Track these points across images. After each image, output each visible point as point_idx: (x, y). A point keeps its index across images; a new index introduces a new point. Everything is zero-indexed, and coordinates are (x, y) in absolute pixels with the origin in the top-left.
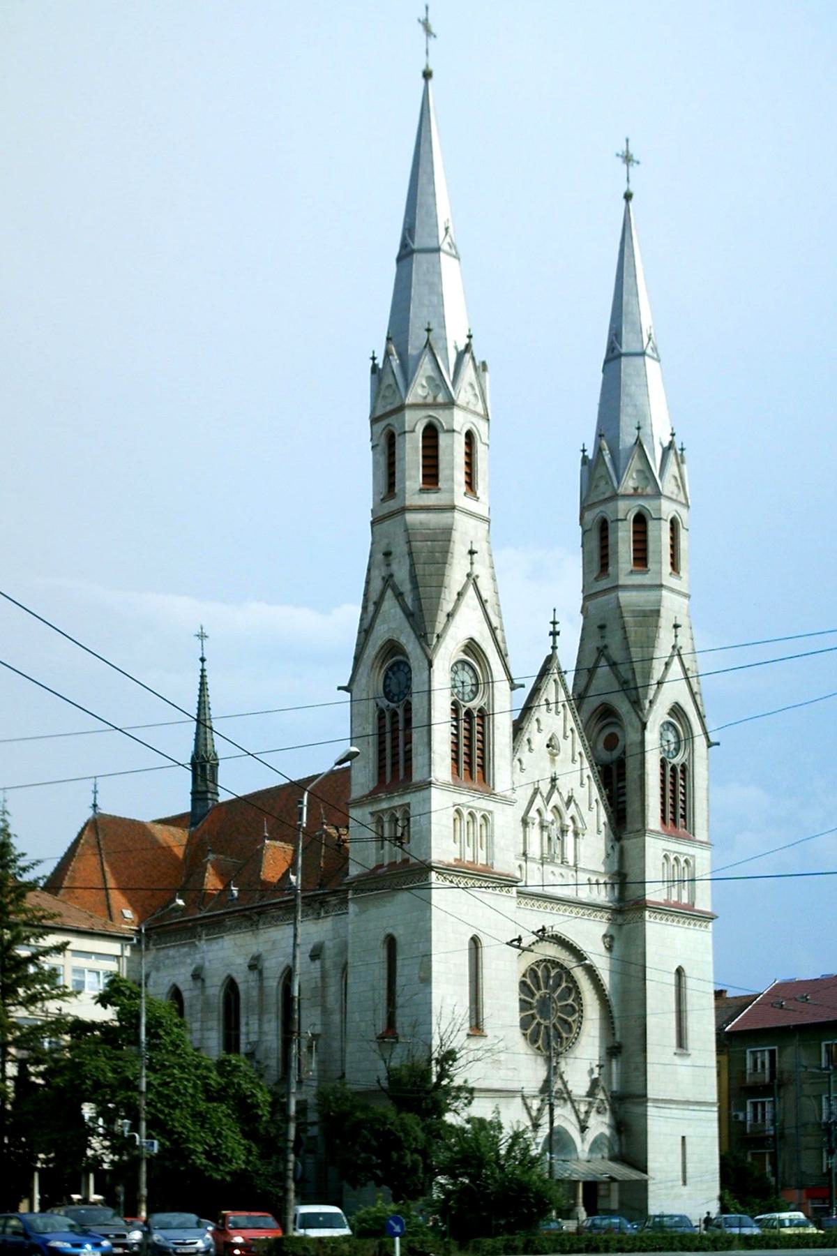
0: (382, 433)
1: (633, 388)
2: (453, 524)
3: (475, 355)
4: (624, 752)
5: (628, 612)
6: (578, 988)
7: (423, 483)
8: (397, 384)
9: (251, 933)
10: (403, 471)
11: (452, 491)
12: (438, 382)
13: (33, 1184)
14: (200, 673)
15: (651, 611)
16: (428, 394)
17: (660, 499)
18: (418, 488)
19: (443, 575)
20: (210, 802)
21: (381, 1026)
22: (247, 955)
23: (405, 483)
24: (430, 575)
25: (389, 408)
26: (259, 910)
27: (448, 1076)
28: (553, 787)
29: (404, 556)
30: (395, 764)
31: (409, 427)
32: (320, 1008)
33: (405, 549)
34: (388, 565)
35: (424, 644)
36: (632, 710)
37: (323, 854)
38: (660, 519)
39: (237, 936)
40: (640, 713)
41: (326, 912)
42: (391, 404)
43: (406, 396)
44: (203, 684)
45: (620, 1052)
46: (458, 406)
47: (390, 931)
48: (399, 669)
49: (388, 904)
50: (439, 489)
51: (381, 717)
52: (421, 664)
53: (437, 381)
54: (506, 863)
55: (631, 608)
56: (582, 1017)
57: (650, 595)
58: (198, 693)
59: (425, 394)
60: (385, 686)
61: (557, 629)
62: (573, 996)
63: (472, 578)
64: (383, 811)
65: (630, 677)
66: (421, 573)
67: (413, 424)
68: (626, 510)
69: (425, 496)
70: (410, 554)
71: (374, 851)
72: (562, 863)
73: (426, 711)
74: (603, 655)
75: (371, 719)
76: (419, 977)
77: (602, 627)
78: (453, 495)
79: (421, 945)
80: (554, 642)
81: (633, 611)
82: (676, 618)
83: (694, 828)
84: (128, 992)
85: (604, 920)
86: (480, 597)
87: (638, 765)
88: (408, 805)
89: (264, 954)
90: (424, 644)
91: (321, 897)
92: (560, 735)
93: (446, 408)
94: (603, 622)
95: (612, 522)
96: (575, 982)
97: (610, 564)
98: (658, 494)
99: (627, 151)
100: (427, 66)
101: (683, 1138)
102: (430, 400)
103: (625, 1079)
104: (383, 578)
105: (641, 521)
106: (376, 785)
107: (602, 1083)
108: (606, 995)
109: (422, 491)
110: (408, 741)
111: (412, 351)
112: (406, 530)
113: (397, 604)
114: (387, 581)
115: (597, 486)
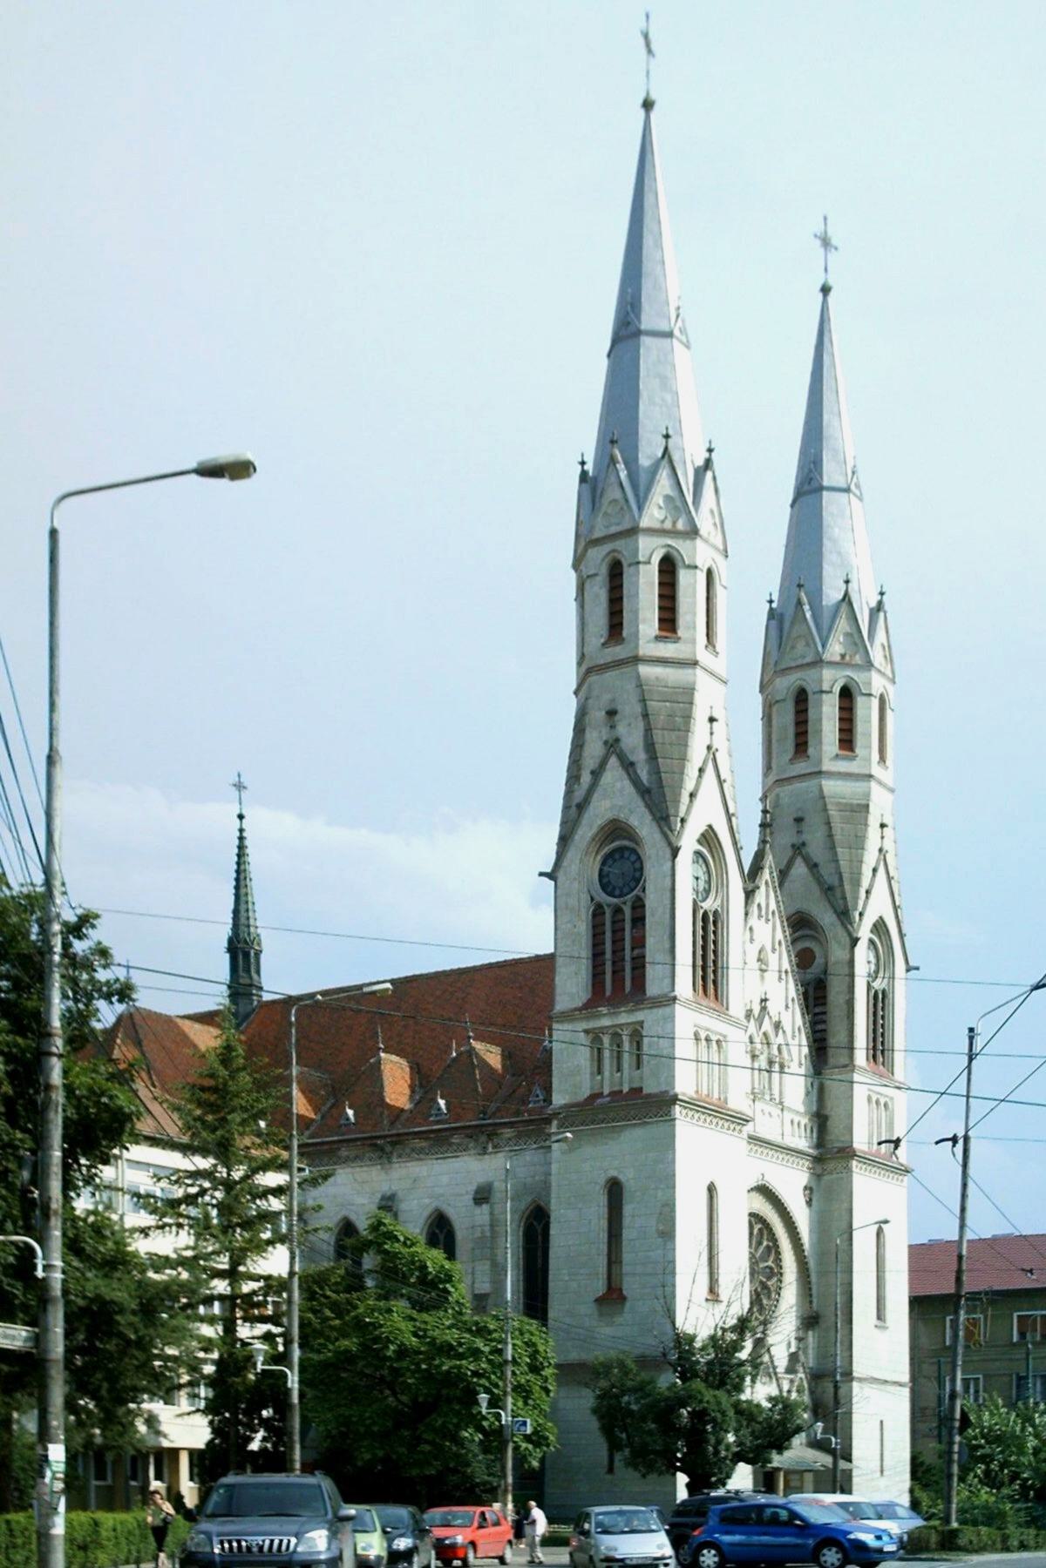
0: (603, 560)
1: (837, 530)
2: (694, 683)
3: (716, 474)
4: (825, 972)
5: (832, 804)
6: (778, 1247)
7: (660, 629)
8: (627, 501)
9: (379, 1167)
10: (636, 612)
11: (693, 642)
12: (679, 504)
14: (238, 834)
15: (858, 805)
16: (666, 518)
17: (870, 670)
18: (654, 635)
19: (686, 745)
20: (255, 998)
21: (600, 1287)
22: (373, 1194)
23: (638, 626)
24: (671, 744)
25: (613, 530)
26: (394, 1139)
27: (388, 1341)
28: (764, 1009)
29: (637, 717)
30: (618, 972)
31: (643, 556)
32: (488, 1263)
33: (638, 709)
34: (613, 727)
35: (666, 829)
36: (838, 923)
37: (478, 1077)
38: (870, 695)
39: (358, 1169)
40: (849, 926)
41: (495, 1147)
42: (618, 524)
43: (640, 516)
44: (241, 847)
45: (817, 1323)
46: (701, 537)
47: (613, 1173)
48: (622, 857)
49: (611, 1142)
50: (679, 638)
51: (598, 912)
52: (661, 853)
53: (677, 504)
54: (738, 1101)
55: (836, 800)
56: (781, 1282)
57: (858, 787)
58: (236, 859)
59: (662, 518)
60: (601, 876)
62: (772, 1259)
64: (603, 1030)
65: (836, 883)
66: (660, 741)
67: (648, 553)
68: (832, 680)
69: (661, 645)
70: (646, 716)
71: (588, 1076)
72: (771, 1100)
73: (668, 911)
74: (800, 853)
75: (584, 917)
76: (657, 1230)
77: (799, 820)
78: (695, 647)
79: (660, 1193)
81: (839, 804)
82: (882, 815)
83: (893, 1066)
84: (402, 1239)
85: (805, 1169)
86: (718, 776)
87: (844, 987)
88: (641, 1023)
89: (400, 1194)
90: (666, 829)
91: (490, 1128)
92: (769, 948)
93: (687, 538)
94: (800, 814)
95: (814, 693)
96: (776, 1240)
97: (810, 743)
98: (869, 665)
99: (826, 232)
100: (648, 94)
101: (882, 1422)
102: (668, 525)
103: (824, 1353)
104: (606, 743)
105: (847, 694)
106: (589, 996)
107: (802, 1358)
108: (805, 1257)
109: (657, 638)
110: (639, 942)
111: (645, 461)
112: (640, 686)
113: (626, 776)
114: (612, 746)
115: (793, 647)
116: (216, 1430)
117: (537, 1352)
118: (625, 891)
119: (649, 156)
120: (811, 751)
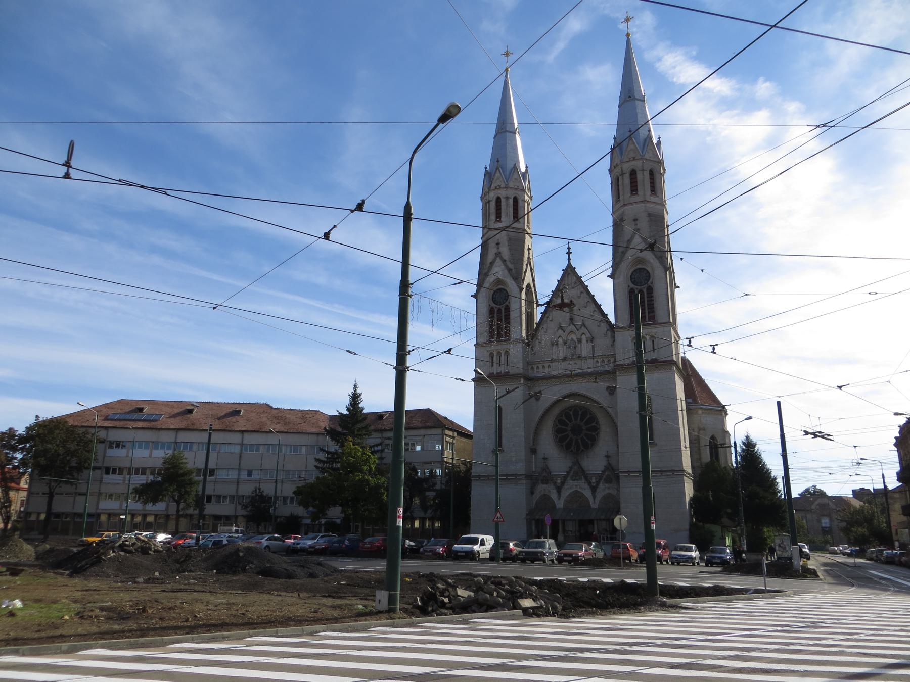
34: (498, 248)
80: (569, 257)
118: (505, 301)
119: (846, 563)
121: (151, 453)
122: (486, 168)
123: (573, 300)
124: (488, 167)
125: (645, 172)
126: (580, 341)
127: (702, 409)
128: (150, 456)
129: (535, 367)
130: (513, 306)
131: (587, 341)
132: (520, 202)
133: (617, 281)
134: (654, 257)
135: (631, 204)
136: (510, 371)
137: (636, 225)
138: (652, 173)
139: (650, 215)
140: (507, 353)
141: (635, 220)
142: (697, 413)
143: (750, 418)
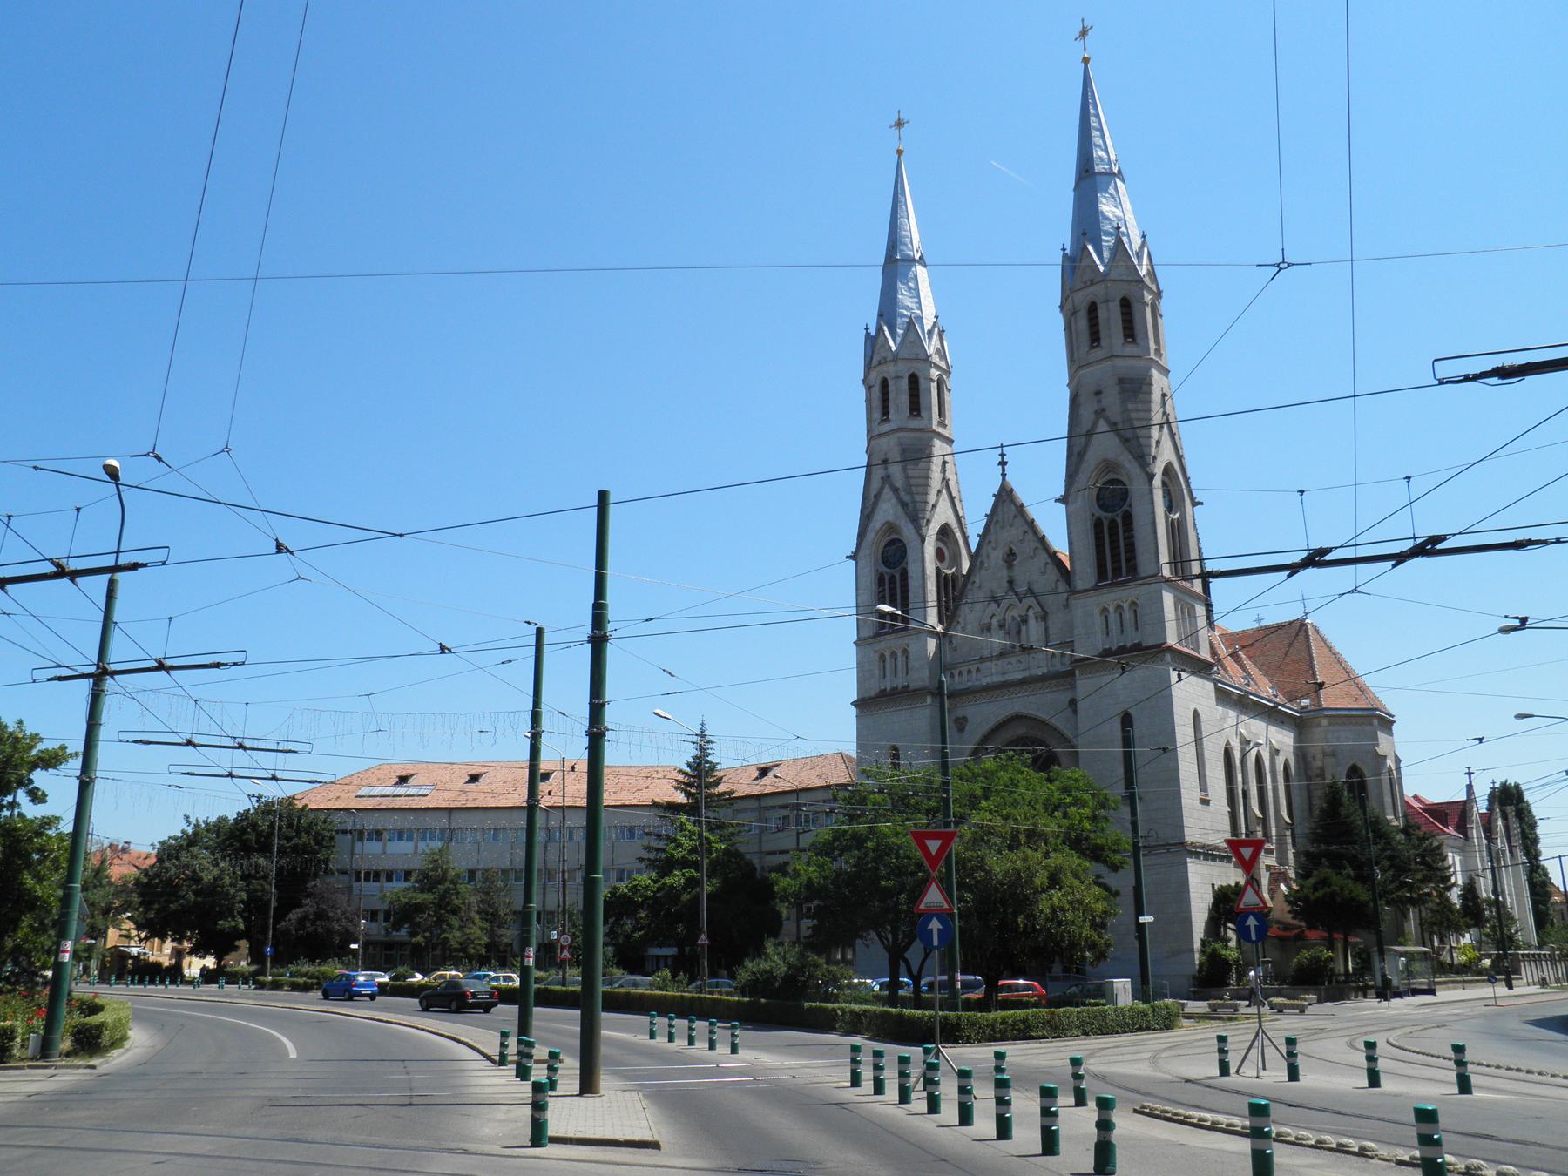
13: (404, 1031)
61: (1005, 460)
63: (945, 481)
80: (1003, 470)
116: (855, 940)
117: (919, 813)
120: (923, 413)
121: (416, 847)
122: (1064, 249)
123: (1014, 548)
124: (1068, 247)
125: (1111, 304)
126: (1025, 621)
127: (1327, 716)
128: (416, 852)
129: (956, 672)
130: (913, 569)
131: (1037, 619)
132: (922, 382)
133: (1072, 508)
134: (1131, 457)
135: (1089, 364)
136: (911, 685)
137: (1099, 402)
138: (1126, 304)
139: (1121, 381)
140: (905, 652)
141: (1098, 393)
142: (1319, 725)
143: (1520, 717)
